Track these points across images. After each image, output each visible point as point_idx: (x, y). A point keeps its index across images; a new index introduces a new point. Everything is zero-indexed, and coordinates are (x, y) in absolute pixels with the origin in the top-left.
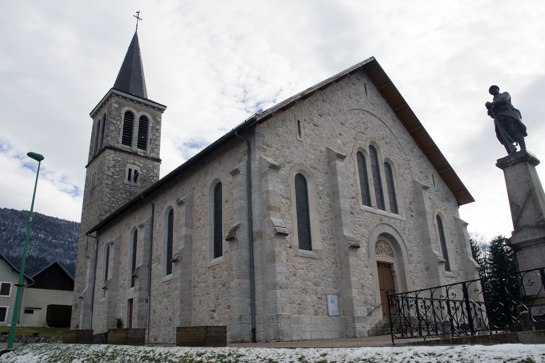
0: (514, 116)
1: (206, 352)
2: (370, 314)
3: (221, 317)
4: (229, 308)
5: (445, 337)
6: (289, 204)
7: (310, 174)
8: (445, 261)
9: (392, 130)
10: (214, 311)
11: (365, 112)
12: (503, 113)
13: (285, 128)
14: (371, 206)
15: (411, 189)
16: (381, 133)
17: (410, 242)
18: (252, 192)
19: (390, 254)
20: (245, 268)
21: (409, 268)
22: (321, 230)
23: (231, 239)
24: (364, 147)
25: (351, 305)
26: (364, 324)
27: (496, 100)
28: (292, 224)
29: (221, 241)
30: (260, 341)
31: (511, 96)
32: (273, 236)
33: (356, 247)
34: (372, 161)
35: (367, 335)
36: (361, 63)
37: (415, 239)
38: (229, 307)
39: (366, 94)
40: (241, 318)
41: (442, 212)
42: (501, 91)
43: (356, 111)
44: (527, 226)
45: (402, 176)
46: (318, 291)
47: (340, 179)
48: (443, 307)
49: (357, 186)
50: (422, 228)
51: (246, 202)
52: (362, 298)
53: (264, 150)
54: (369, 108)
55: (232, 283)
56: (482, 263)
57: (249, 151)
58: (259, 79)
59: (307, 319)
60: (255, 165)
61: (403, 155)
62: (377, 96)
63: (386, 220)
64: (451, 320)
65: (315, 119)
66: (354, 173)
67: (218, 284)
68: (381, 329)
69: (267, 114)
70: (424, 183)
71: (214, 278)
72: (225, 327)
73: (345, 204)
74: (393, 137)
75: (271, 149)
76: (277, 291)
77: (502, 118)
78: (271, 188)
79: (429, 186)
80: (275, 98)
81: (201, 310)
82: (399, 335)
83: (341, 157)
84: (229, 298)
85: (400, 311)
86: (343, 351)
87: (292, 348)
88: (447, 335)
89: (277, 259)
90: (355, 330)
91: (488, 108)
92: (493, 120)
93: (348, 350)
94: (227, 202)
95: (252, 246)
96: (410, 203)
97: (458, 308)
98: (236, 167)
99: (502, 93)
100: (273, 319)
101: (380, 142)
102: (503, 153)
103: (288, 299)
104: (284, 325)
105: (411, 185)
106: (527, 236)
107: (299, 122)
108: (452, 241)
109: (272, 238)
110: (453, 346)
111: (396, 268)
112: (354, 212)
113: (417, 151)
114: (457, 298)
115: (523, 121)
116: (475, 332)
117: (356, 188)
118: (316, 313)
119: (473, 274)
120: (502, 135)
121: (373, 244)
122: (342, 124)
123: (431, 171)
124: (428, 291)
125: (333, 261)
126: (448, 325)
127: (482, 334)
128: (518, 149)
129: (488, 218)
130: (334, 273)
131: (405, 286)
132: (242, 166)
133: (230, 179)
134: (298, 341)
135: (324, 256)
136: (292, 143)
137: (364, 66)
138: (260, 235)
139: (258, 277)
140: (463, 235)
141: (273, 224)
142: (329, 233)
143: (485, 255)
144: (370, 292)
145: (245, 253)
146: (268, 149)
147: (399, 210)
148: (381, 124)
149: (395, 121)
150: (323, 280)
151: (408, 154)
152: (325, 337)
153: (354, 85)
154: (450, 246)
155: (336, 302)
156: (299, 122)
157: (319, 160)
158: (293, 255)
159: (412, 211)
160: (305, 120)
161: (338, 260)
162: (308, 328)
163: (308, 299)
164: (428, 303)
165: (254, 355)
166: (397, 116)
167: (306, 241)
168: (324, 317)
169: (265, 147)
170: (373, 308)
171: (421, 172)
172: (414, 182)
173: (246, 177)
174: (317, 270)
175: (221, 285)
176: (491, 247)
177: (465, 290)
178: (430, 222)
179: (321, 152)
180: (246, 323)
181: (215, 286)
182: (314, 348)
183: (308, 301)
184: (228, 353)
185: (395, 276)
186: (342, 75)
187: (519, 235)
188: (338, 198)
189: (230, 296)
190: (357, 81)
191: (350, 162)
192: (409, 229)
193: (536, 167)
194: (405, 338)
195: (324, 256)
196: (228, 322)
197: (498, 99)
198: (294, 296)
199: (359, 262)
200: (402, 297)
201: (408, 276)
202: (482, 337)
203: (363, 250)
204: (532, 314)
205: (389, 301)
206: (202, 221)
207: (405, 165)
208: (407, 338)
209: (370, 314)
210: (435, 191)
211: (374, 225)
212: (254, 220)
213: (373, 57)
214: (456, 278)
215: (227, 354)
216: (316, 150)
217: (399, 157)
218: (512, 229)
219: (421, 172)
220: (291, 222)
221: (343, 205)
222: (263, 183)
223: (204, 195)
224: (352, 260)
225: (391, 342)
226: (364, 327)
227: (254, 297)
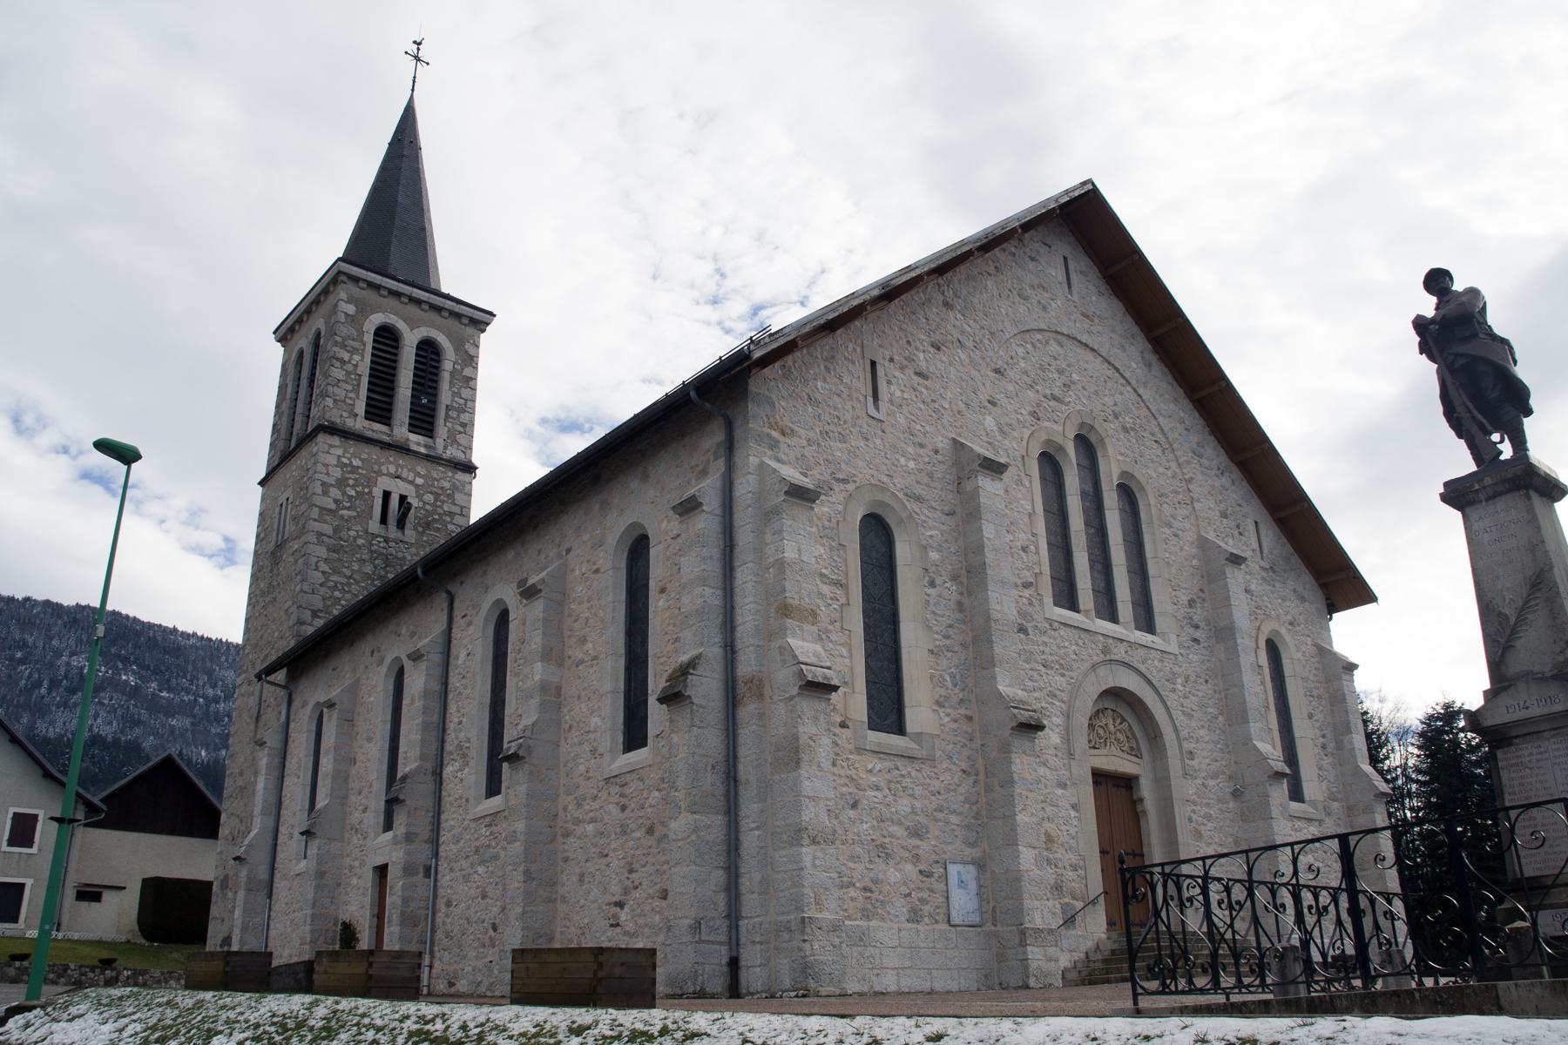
1: (597, 1022)
2: (1069, 921)
3: (641, 921)
4: (665, 898)
5: (1286, 993)
6: (843, 600)
7: (904, 515)
8: (1288, 771)
9: (1141, 391)
10: (620, 905)
11: (1064, 339)
12: (1461, 349)
13: (835, 382)
15: (1195, 562)
16: (1109, 400)
17: (1190, 716)
18: (737, 564)
19: (1132, 748)
20: (712, 782)
21: (1184, 789)
22: (932, 677)
23: (672, 697)
25: (1016, 893)
26: (1052, 951)
27: (1443, 311)
28: (851, 657)
29: (646, 702)
32: (795, 690)
33: (1031, 728)
36: (1056, 198)
37: (1202, 706)
38: (664, 895)
40: (697, 926)
41: (1283, 631)
42: (1458, 286)
43: (1039, 336)
44: (1528, 676)
45: (1169, 525)
46: (921, 852)
47: (988, 530)
48: (1283, 906)
49: (1037, 553)
50: (1225, 675)
51: (719, 592)
52: (1049, 874)
53: (774, 445)
54: (1076, 327)
55: (673, 825)
56: (1396, 779)
57: (730, 447)
58: (760, 236)
59: (888, 932)
60: (745, 487)
61: (1173, 465)
62: (1101, 294)
63: (1119, 652)
64: (1305, 944)
67: (633, 826)
68: (1099, 965)
69: (782, 341)
70: (1231, 546)
71: (624, 808)
72: (653, 952)
73: (1003, 604)
74: (1145, 412)
75: (793, 441)
76: (804, 850)
77: (1461, 361)
78: (790, 554)
79: (1247, 554)
80: (804, 293)
81: (582, 902)
82: (1154, 985)
83: (994, 468)
84: (666, 867)
85: (1157, 913)
86: (992, 1028)
87: (843, 1016)
88: (1292, 988)
89: (805, 758)
90: (1026, 967)
92: (1435, 366)
93: (1007, 1024)
94: (663, 591)
95: (734, 720)
96: (1191, 603)
97: (1325, 908)
98: (692, 491)
99: (1460, 289)
100: (790, 930)
101: (1106, 425)
102: (1462, 463)
103: (835, 875)
104: (819, 949)
105: (1194, 551)
106: (1528, 704)
107: (873, 364)
108: (1310, 716)
109: (791, 698)
110: (1309, 1020)
111: (1146, 790)
113: (1214, 455)
114: (1321, 881)
115: (1522, 372)
116: (1374, 979)
118: (915, 916)
119: (1369, 810)
120: (1461, 410)
121: (1081, 720)
122: (997, 371)
123: (1252, 511)
124: (1241, 859)
125: (964, 765)
126: (1296, 959)
127: (1393, 984)
128: (1507, 451)
129: (1417, 649)
130: (967, 800)
131: (1171, 841)
132: (708, 489)
133: (673, 524)
134: (861, 994)
135: (939, 753)
136: (854, 425)
137: (1063, 207)
138: (758, 687)
139: (750, 809)
140: (1344, 699)
143: (1404, 755)
144: (1072, 858)
145: (714, 740)
146: (784, 442)
147: (1159, 622)
148: (1111, 372)
149: (1149, 366)
151: (1188, 462)
152: (938, 986)
153: (1032, 259)
154: (1301, 728)
155: (973, 885)
156: (873, 364)
158: (851, 747)
159: (1197, 627)
160: (891, 360)
162: (891, 960)
163: (893, 876)
164: (1239, 893)
166: (1156, 351)
167: (888, 709)
168: (937, 927)
169: (775, 434)
170: (1079, 905)
171: (1224, 515)
172: (1203, 543)
173: (718, 520)
174: (918, 790)
175: (643, 830)
176: (1422, 735)
177: (1346, 856)
178: (1246, 660)
179: (936, 452)
180: (712, 942)
181: (624, 833)
182: (909, 1017)
183: (892, 880)
184: (658, 1028)
185: (1144, 812)
186: (999, 232)
187: (1504, 700)
188: (983, 585)
189: (667, 862)
190: (1043, 249)
191: (1020, 482)
192: (1187, 679)
193: (1556, 505)
194: (1171, 993)
195: (939, 753)
196: (661, 938)
197: (1451, 307)
198: (851, 865)
199: (1042, 771)
200: (1163, 874)
201: (1181, 812)
202: (1395, 993)
203: (1051, 737)
205: (1125, 884)
207: (1176, 492)
208: (1177, 992)
209: (1069, 921)
211: (1087, 665)
212: (739, 645)
213: (1090, 181)
214: (1320, 822)
215: (655, 1030)
216: (921, 446)
217: (1161, 470)
218: (1487, 686)
219: (1224, 515)
220: (845, 653)
221: (998, 607)
222: (768, 538)
223: (597, 571)
224: (1021, 764)
225: (1129, 1004)
226: (1052, 959)
227: (737, 867)
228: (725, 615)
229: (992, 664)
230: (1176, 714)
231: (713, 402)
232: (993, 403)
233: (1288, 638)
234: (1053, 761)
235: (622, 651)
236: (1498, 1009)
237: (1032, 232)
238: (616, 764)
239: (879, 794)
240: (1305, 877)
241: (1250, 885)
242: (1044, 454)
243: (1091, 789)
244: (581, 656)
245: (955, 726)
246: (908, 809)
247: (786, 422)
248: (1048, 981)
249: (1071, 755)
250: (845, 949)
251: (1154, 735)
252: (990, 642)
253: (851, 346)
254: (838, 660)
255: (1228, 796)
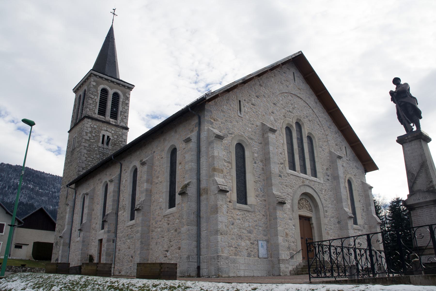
0: (412, 103)
1: (160, 284)
2: (292, 257)
4: (180, 249)
6: (230, 167)
7: (248, 144)
8: (353, 216)
9: (314, 110)
10: (167, 251)
13: (229, 106)
14: (296, 171)
16: (305, 113)
17: (326, 201)
18: (201, 156)
20: (193, 217)
21: (324, 221)
22: (255, 189)
23: (183, 193)
24: (291, 123)
25: (277, 250)
26: (287, 265)
27: (398, 89)
28: (232, 183)
29: (175, 195)
30: (203, 276)
31: (410, 86)
32: (217, 192)
33: (282, 203)
34: (297, 135)
35: (289, 274)
36: (291, 56)
37: (330, 198)
38: (179, 248)
39: (295, 81)
40: (188, 257)
41: (352, 177)
42: (402, 82)
43: (286, 94)
44: (419, 191)
45: (321, 148)
47: (271, 148)
48: (351, 254)
49: (285, 155)
50: (336, 190)
51: (196, 164)
52: (286, 244)
53: (212, 123)
54: (296, 92)
55: (182, 229)
56: (383, 219)
57: (199, 124)
58: (209, 65)
59: (241, 259)
60: (204, 135)
61: (323, 131)
62: (303, 83)
63: (307, 183)
64: (357, 264)
65: (253, 99)
66: (283, 144)
68: (300, 270)
69: (214, 95)
70: (338, 154)
71: (168, 224)
73: (275, 169)
74: (315, 116)
75: (217, 123)
76: (219, 236)
77: (402, 104)
78: (216, 154)
79: (343, 156)
80: (221, 81)
81: (157, 250)
82: (315, 275)
83: (273, 131)
84: (180, 241)
85: (316, 255)
87: (229, 283)
88: (353, 276)
89: (219, 211)
90: (280, 270)
91: (391, 95)
93: (274, 286)
94: (180, 164)
95: (200, 200)
96: (327, 169)
97: (363, 255)
98: (189, 136)
101: (304, 119)
102: (403, 132)
103: (227, 244)
104: (222, 264)
105: (328, 155)
106: (419, 199)
107: (240, 101)
108: (360, 201)
109: (216, 194)
111: (314, 221)
112: (282, 175)
113: (334, 128)
114: (362, 247)
115: (419, 106)
116: (376, 274)
117: (284, 156)
118: (249, 255)
119: (375, 227)
120: (402, 117)
122: (274, 104)
123: (344, 144)
124: (340, 241)
125: (263, 213)
126: (354, 268)
127: (381, 276)
128: (415, 128)
129: (389, 183)
130: (264, 223)
132: (193, 135)
133: (184, 145)
134: (234, 277)
137: (293, 58)
138: (206, 191)
139: (204, 225)
141: (217, 182)
142: (261, 191)
143: (385, 212)
144: (293, 240)
145: (194, 205)
146: (214, 123)
147: (318, 174)
148: (306, 105)
149: (316, 103)
150: (255, 229)
152: (255, 275)
153: (284, 73)
154: (357, 204)
155: (265, 247)
156: (240, 101)
157: (255, 133)
159: (329, 176)
160: (245, 100)
161: (268, 213)
162: (242, 267)
163: (243, 244)
164: (339, 250)
165: (198, 287)
167: (242, 197)
169: (212, 121)
170: (295, 253)
171: (337, 145)
172: (331, 153)
173: (196, 144)
174: (251, 220)
175: (174, 230)
176: (390, 207)
177: (369, 240)
178: (342, 185)
179: (257, 126)
181: (168, 231)
182: (247, 283)
183: (243, 245)
184: (177, 285)
185: (313, 227)
186: (275, 65)
188: (269, 163)
189: (180, 239)
191: (280, 135)
192: (326, 190)
193: (428, 144)
194: (320, 277)
197: (400, 89)
198: (232, 241)
199: (285, 215)
200: (318, 244)
201: (323, 227)
202: (382, 278)
203: (288, 206)
204: (422, 261)
205: (307, 247)
206: (160, 179)
208: (321, 277)
209: (292, 257)
210: (347, 160)
211: (298, 186)
212: (201, 179)
213: (301, 52)
215: (176, 286)
216: (253, 124)
217: (319, 132)
219: (337, 145)
222: (210, 149)
223: (162, 158)
224: (279, 213)
225: (308, 280)
226: (287, 267)
227: (200, 241)
228: (198, 171)
229: (271, 185)
230: (323, 200)
231: (196, 110)
232: (273, 113)
233: (354, 179)
234: (288, 213)
235: (169, 180)
236: (410, 283)
237: (284, 65)
238: (167, 212)
239: (240, 221)
240: (357, 246)
241: (342, 248)
242: (287, 127)
243: (298, 220)
244: (157, 181)
245: (261, 202)
246: (248, 226)
247: (215, 117)
248: (286, 274)
249: (293, 211)
250: (230, 264)
251: (316, 206)
252: (271, 179)
253: (234, 96)
254: (229, 184)
255: (336, 223)
